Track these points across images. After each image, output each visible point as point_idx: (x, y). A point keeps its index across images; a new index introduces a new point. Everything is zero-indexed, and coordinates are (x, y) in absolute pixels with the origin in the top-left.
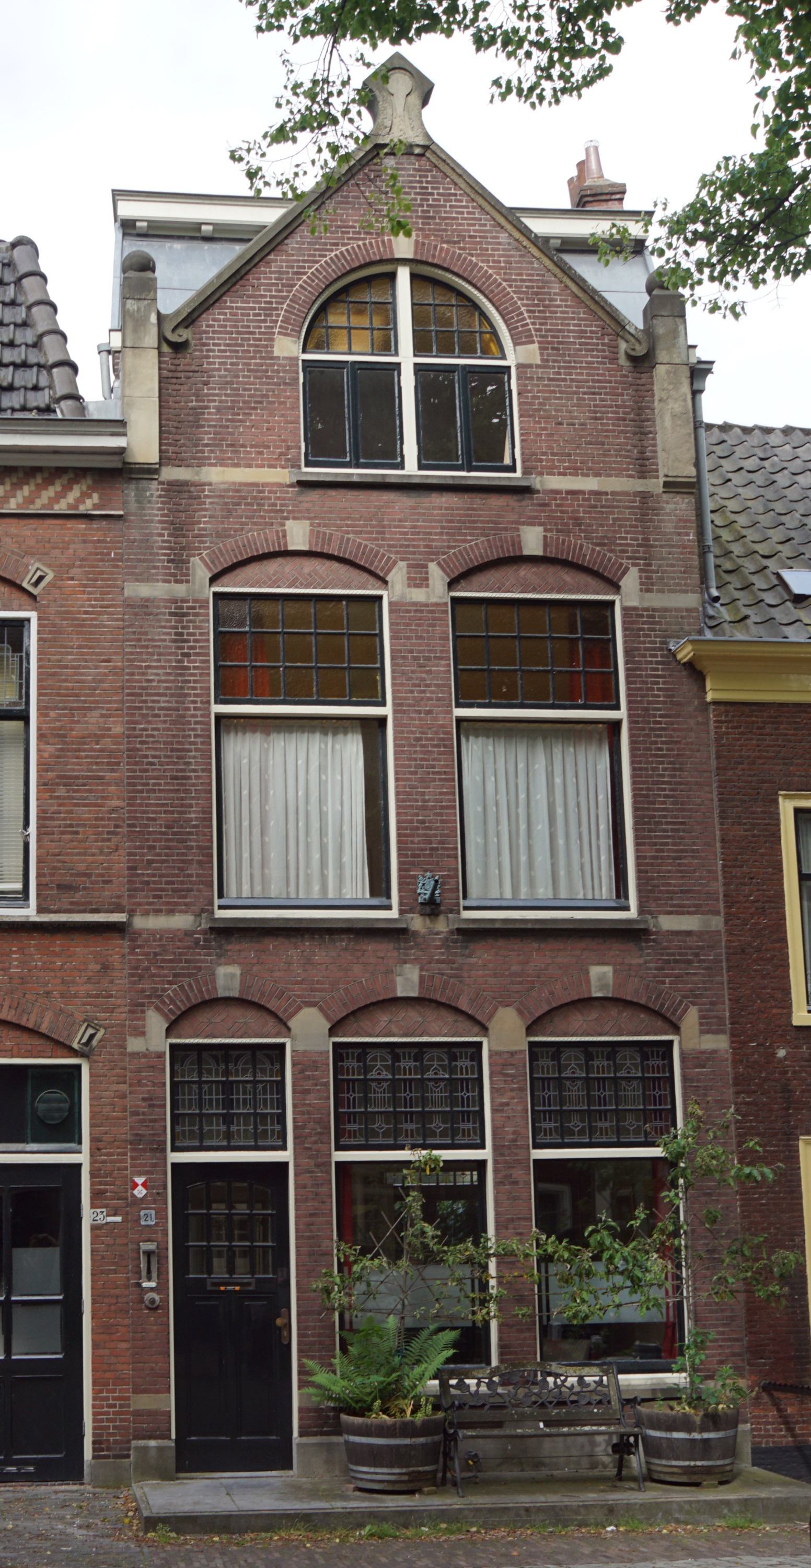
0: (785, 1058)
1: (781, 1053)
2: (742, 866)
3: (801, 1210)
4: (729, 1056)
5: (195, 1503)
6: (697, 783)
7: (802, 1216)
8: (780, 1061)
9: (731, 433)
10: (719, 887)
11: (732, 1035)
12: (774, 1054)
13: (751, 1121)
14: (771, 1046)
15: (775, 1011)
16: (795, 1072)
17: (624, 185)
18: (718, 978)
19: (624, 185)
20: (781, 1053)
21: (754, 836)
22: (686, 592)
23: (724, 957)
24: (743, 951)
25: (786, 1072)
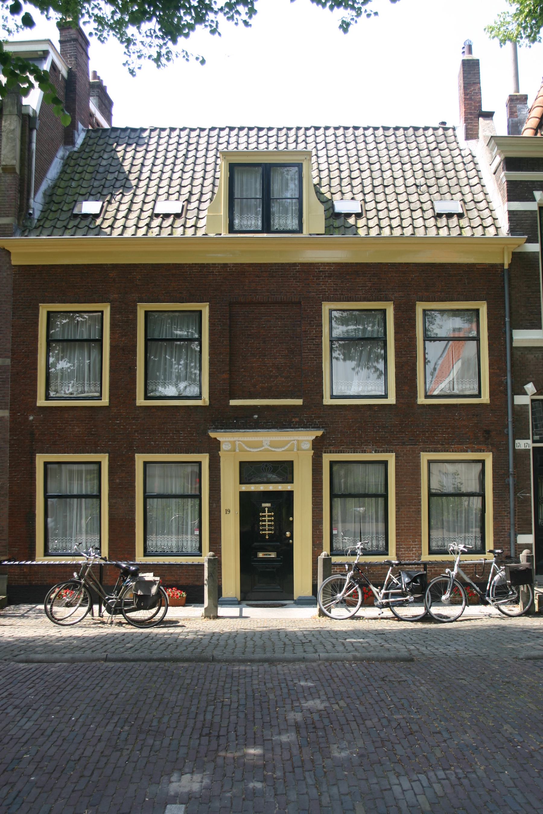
0: (33, 420)
1: (31, 418)
2: (20, 337)
3: (35, 485)
4: (9, 419)
5: (372, 390)
6: (5, 301)
7: (35, 488)
8: (30, 421)
9: (360, 130)
10: (9, 346)
11: (10, 410)
12: (28, 418)
13: (15, 447)
14: (27, 415)
15: (29, 400)
16: (36, 426)
17: (478, 60)
18: (7, 386)
19: (478, 60)
20: (31, 418)
21: (27, 323)
22: (8, 216)
23: (9, 377)
24: (18, 374)
25: (33, 426)
